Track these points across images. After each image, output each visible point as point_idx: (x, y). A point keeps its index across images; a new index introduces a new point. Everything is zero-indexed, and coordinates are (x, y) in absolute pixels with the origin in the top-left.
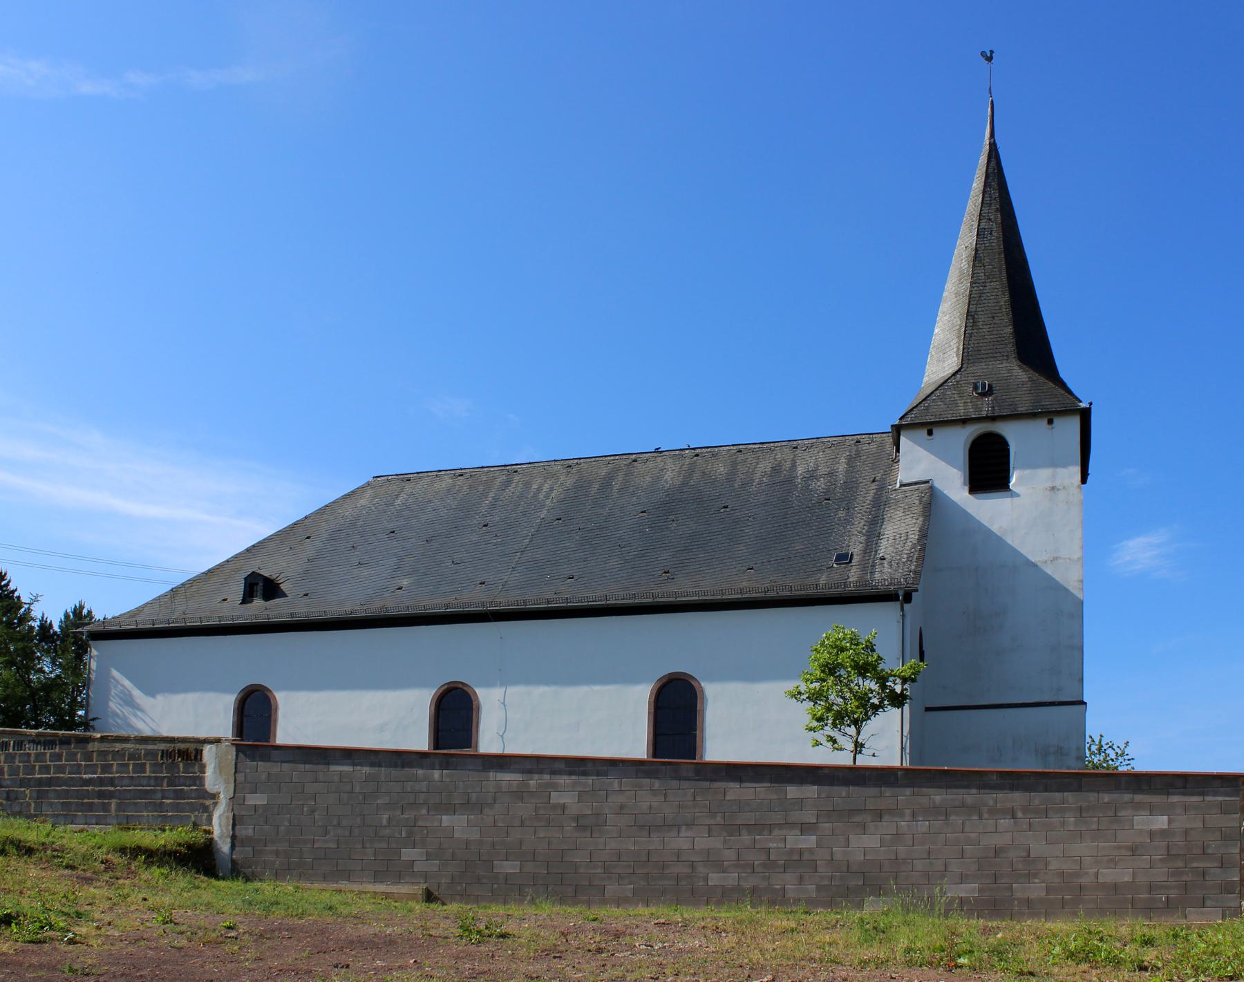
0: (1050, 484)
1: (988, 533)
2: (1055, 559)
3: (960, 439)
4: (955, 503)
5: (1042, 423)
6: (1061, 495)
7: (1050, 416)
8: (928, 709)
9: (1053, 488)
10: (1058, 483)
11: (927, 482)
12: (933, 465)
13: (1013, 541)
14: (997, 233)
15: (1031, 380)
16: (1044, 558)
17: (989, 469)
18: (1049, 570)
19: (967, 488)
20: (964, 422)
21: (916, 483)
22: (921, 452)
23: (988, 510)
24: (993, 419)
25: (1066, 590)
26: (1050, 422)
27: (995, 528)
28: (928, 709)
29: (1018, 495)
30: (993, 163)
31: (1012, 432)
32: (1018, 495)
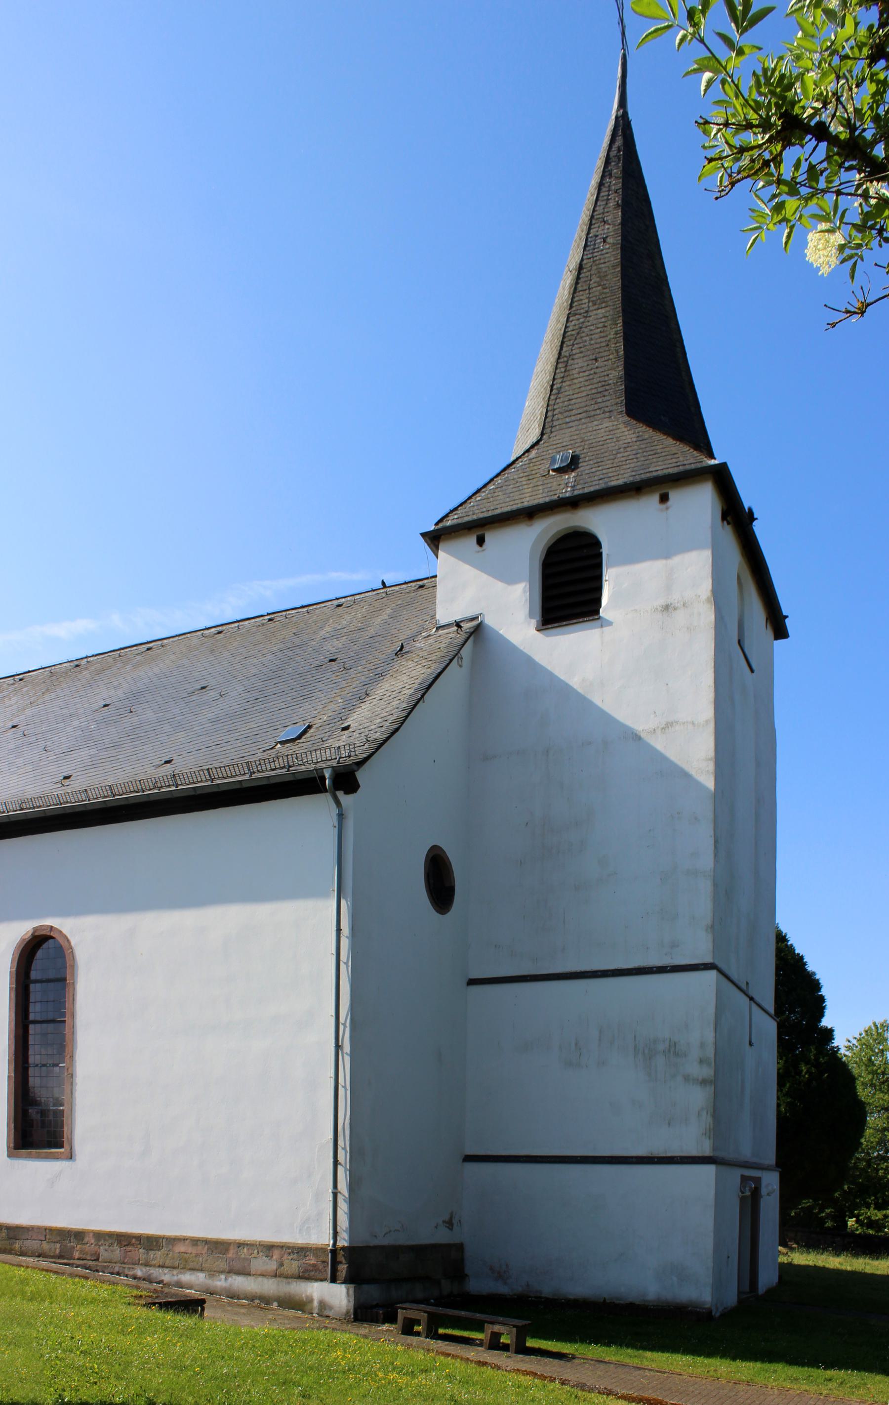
0: (662, 602)
1: (564, 691)
2: (669, 725)
3: (526, 544)
4: (513, 649)
5: (651, 501)
6: (680, 617)
7: (660, 486)
8: (472, 982)
9: (667, 608)
10: (675, 598)
11: (476, 618)
12: (493, 591)
13: (604, 700)
14: (611, 230)
15: (640, 439)
16: (651, 725)
17: (570, 589)
18: (659, 743)
19: (533, 623)
20: (530, 514)
21: (176, 636)
22: (468, 572)
23: (571, 655)
24: (573, 503)
25: (686, 775)
26: (664, 499)
27: (575, 682)
28: (472, 982)
29: (610, 623)
30: (619, 141)
31: (599, 521)
32: (610, 623)
